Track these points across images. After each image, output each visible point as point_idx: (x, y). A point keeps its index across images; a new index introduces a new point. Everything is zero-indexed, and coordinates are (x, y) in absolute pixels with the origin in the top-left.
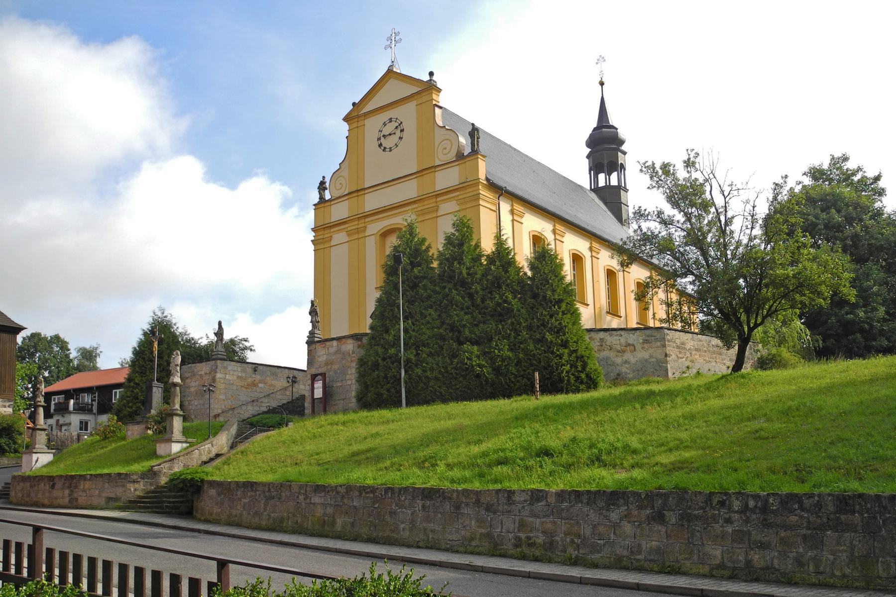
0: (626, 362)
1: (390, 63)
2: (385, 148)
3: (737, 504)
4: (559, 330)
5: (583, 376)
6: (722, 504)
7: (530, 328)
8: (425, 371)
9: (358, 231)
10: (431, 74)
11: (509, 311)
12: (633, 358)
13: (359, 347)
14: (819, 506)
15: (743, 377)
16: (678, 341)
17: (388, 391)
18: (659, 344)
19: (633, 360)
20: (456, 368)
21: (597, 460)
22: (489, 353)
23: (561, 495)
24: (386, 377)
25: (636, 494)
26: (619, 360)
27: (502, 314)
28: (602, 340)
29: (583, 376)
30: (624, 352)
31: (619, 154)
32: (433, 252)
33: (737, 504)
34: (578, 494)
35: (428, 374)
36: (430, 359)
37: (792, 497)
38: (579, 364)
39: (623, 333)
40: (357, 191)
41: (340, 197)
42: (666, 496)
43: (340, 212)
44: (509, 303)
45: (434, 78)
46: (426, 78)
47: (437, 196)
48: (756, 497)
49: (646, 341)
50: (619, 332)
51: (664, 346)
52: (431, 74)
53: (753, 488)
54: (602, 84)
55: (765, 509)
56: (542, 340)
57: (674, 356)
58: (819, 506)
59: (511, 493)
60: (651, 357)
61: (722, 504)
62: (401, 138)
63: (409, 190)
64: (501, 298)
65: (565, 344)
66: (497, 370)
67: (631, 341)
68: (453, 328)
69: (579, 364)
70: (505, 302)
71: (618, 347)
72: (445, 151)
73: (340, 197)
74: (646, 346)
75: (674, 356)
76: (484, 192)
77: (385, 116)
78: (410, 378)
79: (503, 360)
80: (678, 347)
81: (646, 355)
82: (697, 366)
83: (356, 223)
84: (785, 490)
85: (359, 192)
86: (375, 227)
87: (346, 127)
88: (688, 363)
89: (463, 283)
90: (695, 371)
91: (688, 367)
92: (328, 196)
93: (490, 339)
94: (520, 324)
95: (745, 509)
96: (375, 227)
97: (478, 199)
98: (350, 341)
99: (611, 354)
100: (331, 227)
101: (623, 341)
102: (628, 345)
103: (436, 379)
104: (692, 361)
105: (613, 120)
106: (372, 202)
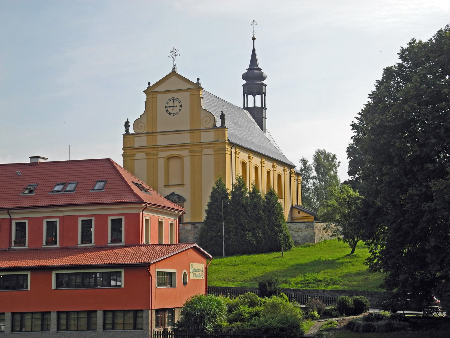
0: (299, 236)
1: (172, 67)
2: (174, 114)
3: (367, 293)
4: (279, 226)
5: (288, 244)
6: (364, 293)
7: (268, 225)
8: (232, 242)
9: (154, 154)
10: (198, 79)
11: (261, 218)
12: (301, 234)
13: (194, 228)
14: (381, 294)
15: (355, 256)
16: (318, 227)
17: (217, 249)
18: (312, 229)
19: (301, 235)
20: (243, 241)
21: (334, 283)
22: (255, 235)
23: (331, 291)
24: (216, 244)
25: (347, 291)
26: (296, 235)
27: (258, 219)
28: (289, 226)
29: (288, 244)
30: (298, 231)
31: (263, 86)
32: (229, 191)
33: (367, 293)
34: (335, 291)
35: (234, 243)
36: (233, 237)
37: (376, 292)
38: (287, 239)
39: (298, 224)
40: (153, 133)
41: (140, 134)
42: (353, 292)
43: (141, 142)
44: (261, 215)
45: (199, 82)
46: (195, 81)
47: (202, 145)
48: (370, 292)
49: (307, 227)
50: (296, 223)
51: (314, 229)
52: (198, 79)
53: (369, 290)
54: (254, 39)
55: (372, 294)
56: (273, 230)
57: (317, 234)
58: (381, 294)
59: (318, 290)
60: (308, 234)
61: (364, 293)
62: (180, 110)
63: (186, 138)
64: (258, 212)
65: (281, 232)
66: (258, 242)
67: (301, 227)
68: (240, 225)
69: (287, 239)
70: (259, 214)
71: (296, 230)
72: (206, 123)
73: (140, 134)
74: (307, 229)
75: (317, 234)
76: (228, 147)
77: (171, 96)
78: (227, 245)
79: (260, 238)
80: (318, 229)
81: (306, 233)
82: (325, 237)
83: (152, 150)
84: (375, 291)
85: (155, 133)
86: (164, 154)
87: (145, 96)
88: (321, 236)
89: (243, 206)
90: (324, 239)
91: (321, 238)
92: (131, 131)
93: (254, 229)
94: (265, 223)
95: (368, 294)
96: (164, 154)
97: (225, 150)
98: (189, 225)
99: (293, 232)
100: (202, 145)
101: (298, 227)
102: (300, 229)
103: (236, 245)
104: (323, 235)
105: (260, 65)
106: (161, 140)
